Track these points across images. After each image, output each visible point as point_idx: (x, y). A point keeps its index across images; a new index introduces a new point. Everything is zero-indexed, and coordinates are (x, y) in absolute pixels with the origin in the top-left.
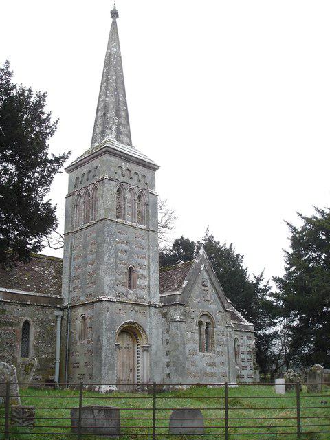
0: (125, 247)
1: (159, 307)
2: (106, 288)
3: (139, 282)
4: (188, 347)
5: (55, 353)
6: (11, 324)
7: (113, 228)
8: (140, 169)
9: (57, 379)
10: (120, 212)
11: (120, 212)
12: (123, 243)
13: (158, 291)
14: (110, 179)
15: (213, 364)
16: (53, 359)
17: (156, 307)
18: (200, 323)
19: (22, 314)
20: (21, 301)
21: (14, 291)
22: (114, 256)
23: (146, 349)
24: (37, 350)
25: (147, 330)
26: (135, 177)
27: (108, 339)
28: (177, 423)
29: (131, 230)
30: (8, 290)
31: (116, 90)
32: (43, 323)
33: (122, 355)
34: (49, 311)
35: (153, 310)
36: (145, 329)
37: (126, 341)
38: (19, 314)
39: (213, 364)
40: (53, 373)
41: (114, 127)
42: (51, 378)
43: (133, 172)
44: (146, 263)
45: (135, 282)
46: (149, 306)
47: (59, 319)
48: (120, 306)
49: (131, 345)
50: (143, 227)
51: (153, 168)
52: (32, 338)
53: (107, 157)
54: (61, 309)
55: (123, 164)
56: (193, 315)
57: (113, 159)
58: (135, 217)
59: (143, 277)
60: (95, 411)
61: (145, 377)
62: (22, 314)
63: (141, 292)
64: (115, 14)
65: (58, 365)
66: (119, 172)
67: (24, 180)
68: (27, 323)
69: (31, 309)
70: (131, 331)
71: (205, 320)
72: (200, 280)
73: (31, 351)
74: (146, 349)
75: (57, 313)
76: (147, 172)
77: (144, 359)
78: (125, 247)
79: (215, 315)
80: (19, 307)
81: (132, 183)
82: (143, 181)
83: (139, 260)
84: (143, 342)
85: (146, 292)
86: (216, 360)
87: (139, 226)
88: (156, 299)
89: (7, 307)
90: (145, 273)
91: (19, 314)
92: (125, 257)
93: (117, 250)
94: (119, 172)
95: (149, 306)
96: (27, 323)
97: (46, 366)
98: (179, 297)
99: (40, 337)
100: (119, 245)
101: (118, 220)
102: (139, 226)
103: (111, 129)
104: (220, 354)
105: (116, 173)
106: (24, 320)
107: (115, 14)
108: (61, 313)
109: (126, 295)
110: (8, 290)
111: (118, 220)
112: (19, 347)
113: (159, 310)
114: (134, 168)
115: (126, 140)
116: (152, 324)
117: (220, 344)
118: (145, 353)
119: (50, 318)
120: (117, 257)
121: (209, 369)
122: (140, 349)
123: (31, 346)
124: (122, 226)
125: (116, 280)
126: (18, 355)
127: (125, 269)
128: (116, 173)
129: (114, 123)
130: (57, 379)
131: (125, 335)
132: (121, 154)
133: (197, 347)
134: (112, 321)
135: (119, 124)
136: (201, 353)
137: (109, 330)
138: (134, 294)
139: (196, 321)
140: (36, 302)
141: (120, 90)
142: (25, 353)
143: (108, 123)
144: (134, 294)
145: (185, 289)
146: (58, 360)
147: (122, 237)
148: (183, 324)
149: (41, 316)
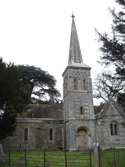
0: (78, 100)
1: (94, 120)
2: (70, 115)
3: (85, 111)
4: (105, 134)
5: (62, 138)
6: (45, 130)
7: (72, 94)
8: (83, 71)
9: (63, 147)
10: (75, 88)
11: (75, 88)
12: (77, 98)
13: (94, 114)
14: (70, 77)
15: (119, 140)
16: (62, 141)
17: (92, 120)
18: (111, 125)
19: (49, 126)
20: (49, 122)
21: (45, 119)
22: (73, 104)
23: (90, 136)
24: (55, 138)
25: (90, 129)
26: (82, 74)
27: (71, 134)
28: (20, 161)
29: (80, 93)
30: (44, 119)
31: (74, 44)
32: (57, 129)
33: (81, 138)
34: (59, 124)
35: (91, 121)
36: (88, 128)
37: (82, 133)
38: (48, 126)
39: (119, 140)
40: (62, 145)
41: (74, 58)
42: (61, 147)
43: (80, 73)
44: (88, 104)
45: (84, 112)
46: (90, 120)
47: (63, 127)
48: (77, 121)
49: (85, 135)
50: (86, 91)
51: (89, 69)
52: (53, 134)
53: (69, 70)
54: (63, 123)
55: (75, 71)
56: (107, 122)
57: (71, 70)
58: (82, 88)
59: (87, 110)
60: (2, 157)
61: (90, 146)
62: (49, 126)
63: (86, 115)
64: (73, 17)
65: (63, 142)
66: (74, 74)
67: (33, 85)
68: (51, 129)
69: (52, 124)
70: (83, 129)
71: (114, 123)
72: (110, 108)
73: (53, 138)
74: (90, 136)
75: (62, 125)
76: (87, 71)
77: (89, 140)
78: (78, 100)
79: (119, 121)
80: (48, 124)
81: (80, 76)
82: (85, 75)
83: (85, 104)
84: (89, 133)
85: (89, 115)
86: (120, 138)
87: (84, 91)
88: (93, 117)
89: (44, 124)
90: (88, 108)
91: (48, 126)
92: (79, 103)
93: (74, 101)
94: (74, 74)
95: (90, 120)
96: (51, 129)
97: (59, 143)
98: (99, 116)
99: (56, 133)
100: (76, 100)
101: (75, 91)
102: (84, 91)
103: (72, 59)
104: (121, 136)
105: (73, 74)
106: (50, 128)
107: (73, 17)
108: (63, 125)
109: (80, 117)
110: (44, 119)
111: (75, 91)
112: (49, 137)
113: (94, 121)
114: (80, 71)
115: (78, 61)
116: (91, 126)
117: (122, 132)
118: (90, 137)
119: (60, 127)
120: (75, 104)
121: (116, 142)
122: (88, 136)
123: (53, 137)
124: (76, 93)
125: (75, 112)
126: (49, 140)
127: (79, 108)
128: (73, 74)
129: (73, 56)
130: (63, 147)
131: (81, 131)
132: (74, 67)
133: (110, 134)
134: (74, 126)
135: (75, 56)
136: (112, 136)
137: (72, 130)
138: (83, 116)
139: (109, 124)
140: (54, 122)
141: (76, 44)
142: (51, 139)
143: (72, 57)
144: (83, 116)
145: (102, 112)
146: (63, 141)
147: (77, 96)
148: (102, 126)
149: (56, 126)
